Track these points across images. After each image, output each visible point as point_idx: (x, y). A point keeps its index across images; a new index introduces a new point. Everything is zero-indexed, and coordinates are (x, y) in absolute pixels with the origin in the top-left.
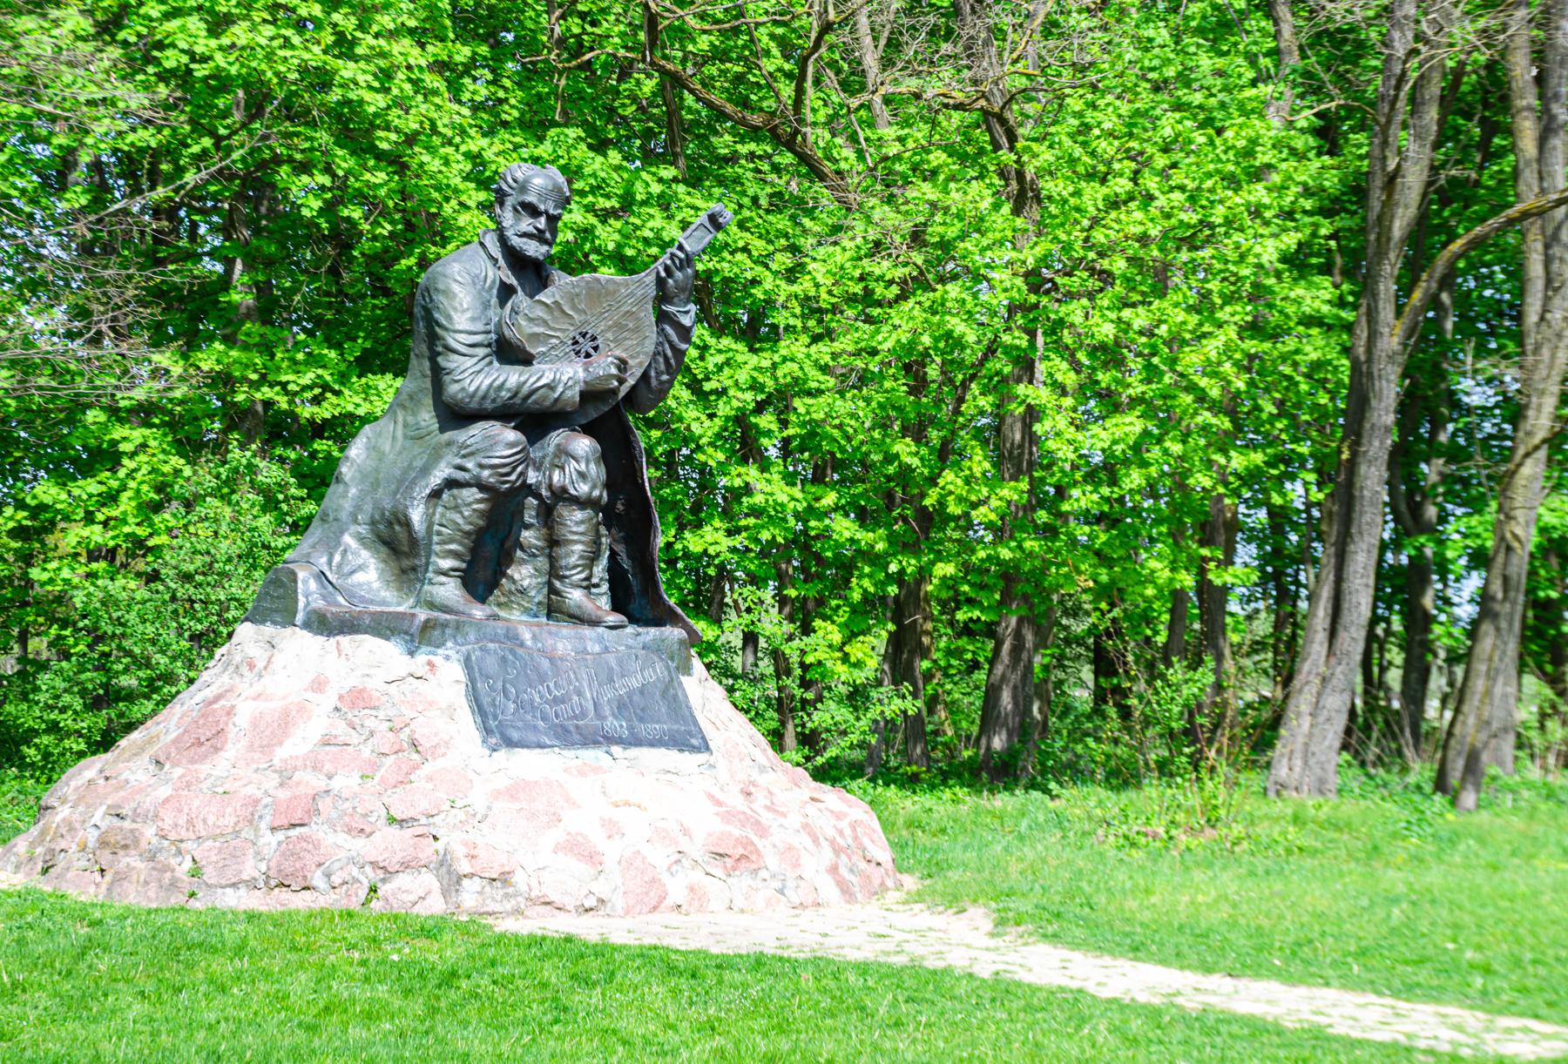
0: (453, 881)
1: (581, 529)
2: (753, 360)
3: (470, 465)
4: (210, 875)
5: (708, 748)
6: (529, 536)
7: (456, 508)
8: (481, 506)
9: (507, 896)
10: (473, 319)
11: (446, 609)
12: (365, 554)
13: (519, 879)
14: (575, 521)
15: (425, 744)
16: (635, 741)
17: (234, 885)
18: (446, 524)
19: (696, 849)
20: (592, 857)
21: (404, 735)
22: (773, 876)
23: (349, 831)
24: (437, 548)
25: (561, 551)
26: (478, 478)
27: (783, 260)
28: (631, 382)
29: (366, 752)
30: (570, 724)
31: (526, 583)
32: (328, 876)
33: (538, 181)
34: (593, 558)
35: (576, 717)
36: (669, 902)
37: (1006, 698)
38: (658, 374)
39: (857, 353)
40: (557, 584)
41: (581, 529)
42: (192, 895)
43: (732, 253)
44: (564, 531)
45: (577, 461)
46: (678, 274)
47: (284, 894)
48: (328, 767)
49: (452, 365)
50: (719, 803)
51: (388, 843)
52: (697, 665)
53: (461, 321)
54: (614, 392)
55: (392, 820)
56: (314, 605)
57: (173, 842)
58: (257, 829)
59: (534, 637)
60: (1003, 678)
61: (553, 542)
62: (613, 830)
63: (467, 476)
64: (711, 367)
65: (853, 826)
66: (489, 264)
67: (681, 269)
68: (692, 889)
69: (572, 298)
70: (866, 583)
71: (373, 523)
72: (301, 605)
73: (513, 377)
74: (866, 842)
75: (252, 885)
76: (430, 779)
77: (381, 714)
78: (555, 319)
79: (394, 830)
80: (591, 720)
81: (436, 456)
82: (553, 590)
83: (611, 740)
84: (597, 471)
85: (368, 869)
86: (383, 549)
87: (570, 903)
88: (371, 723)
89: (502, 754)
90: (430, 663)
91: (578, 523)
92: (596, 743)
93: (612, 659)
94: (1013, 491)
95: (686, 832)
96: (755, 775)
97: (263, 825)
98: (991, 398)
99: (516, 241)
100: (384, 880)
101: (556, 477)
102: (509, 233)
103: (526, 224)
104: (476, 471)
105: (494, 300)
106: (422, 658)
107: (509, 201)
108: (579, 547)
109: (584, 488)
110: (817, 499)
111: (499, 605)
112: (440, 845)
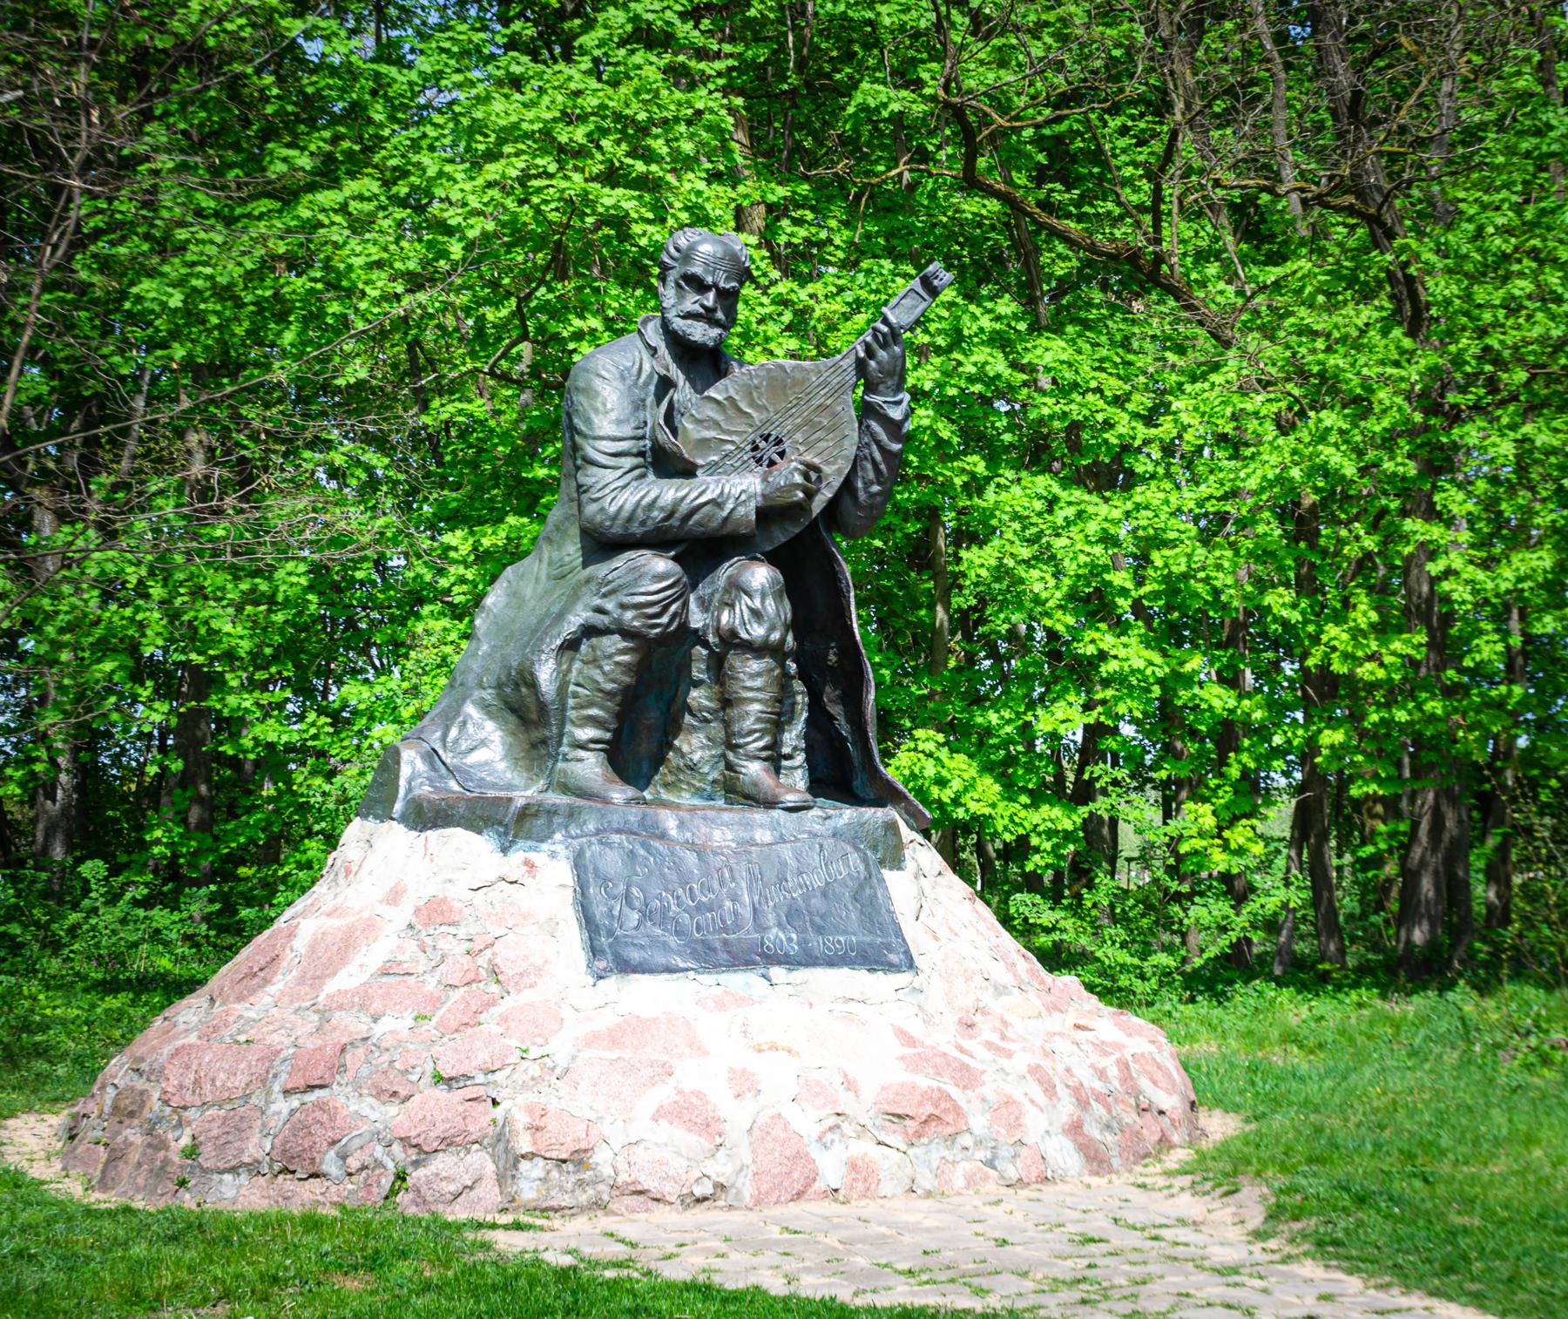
0: (510, 1164)
1: (758, 682)
2: (1103, 510)
3: (610, 605)
4: (208, 1157)
5: (911, 965)
6: (698, 697)
7: (594, 662)
8: (626, 658)
9: (581, 1183)
10: (619, 422)
11: (583, 793)
12: (490, 725)
13: (602, 1158)
14: (752, 674)
15: (508, 970)
16: (808, 959)
17: (233, 1170)
18: (586, 683)
19: (862, 1108)
20: (710, 1127)
21: (482, 961)
22: (979, 1143)
23: (379, 1093)
24: (572, 714)
25: (734, 712)
26: (618, 621)
27: (1141, 402)
28: (826, 494)
29: (431, 984)
30: (715, 940)
31: (696, 757)
32: (343, 1157)
33: (706, 248)
34: (777, 724)
35: (726, 930)
36: (819, 1185)
37: (1426, 885)
38: (867, 484)
39: (1224, 498)
40: (731, 756)
41: (758, 682)
42: (183, 1183)
43: (1083, 394)
44: (736, 688)
45: (754, 596)
46: (882, 354)
47: (287, 1183)
48: (376, 1005)
49: (589, 481)
50: (910, 1041)
51: (434, 1109)
52: (923, 856)
53: (605, 425)
54: (801, 508)
55: (439, 1079)
56: (417, 792)
57: (175, 1110)
58: (269, 1093)
59: (682, 825)
60: (1423, 863)
61: (727, 703)
62: (744, 1084)
63: (606, 619)
64: (1060, 522)
65: (1124, 1066)
66: (646, 355)
67: (884, 346)
68: (854, 1166)
69: (748, 392)
70: (1245, 757)
71: (499, 686)
72: (402, 792)
73: (669, 492)
74: (1144, 1083)
75: (254, 1169)
76: (504, 1019)
77: (462, 932)
78: (728, 419)
79: (440, 1092)
80: (748, 934)
81: (574, 597)
82: (730, 766)
83: (772, 958)
84: (777, 610)
85: (396, 1147)
86: (512, 719)
87: (671, 1190)
88: (444, 944)
89: (612, 983)
90: (527, 863)
91: (753, 676)
92: (749, 964)
93: (786, 852)
94: (1411, 643)
95: (850, 1085)
96: (987, 998)
97: (277, 1088)
98: (1376, 538)
99: (678, 324)
100: (416, 1164)
101: (725, 617)
102: (670, 315)
103: (691, 302)
104: (616, 613)
105: (650, 399)
106: (517, 856)
107: (672, 276)
108: (757, 707)
109: (758, 631)
110: (1182, 664)
111: (666, 785)
112: (499, 1112)
